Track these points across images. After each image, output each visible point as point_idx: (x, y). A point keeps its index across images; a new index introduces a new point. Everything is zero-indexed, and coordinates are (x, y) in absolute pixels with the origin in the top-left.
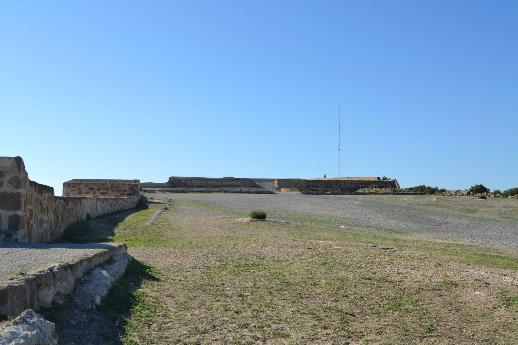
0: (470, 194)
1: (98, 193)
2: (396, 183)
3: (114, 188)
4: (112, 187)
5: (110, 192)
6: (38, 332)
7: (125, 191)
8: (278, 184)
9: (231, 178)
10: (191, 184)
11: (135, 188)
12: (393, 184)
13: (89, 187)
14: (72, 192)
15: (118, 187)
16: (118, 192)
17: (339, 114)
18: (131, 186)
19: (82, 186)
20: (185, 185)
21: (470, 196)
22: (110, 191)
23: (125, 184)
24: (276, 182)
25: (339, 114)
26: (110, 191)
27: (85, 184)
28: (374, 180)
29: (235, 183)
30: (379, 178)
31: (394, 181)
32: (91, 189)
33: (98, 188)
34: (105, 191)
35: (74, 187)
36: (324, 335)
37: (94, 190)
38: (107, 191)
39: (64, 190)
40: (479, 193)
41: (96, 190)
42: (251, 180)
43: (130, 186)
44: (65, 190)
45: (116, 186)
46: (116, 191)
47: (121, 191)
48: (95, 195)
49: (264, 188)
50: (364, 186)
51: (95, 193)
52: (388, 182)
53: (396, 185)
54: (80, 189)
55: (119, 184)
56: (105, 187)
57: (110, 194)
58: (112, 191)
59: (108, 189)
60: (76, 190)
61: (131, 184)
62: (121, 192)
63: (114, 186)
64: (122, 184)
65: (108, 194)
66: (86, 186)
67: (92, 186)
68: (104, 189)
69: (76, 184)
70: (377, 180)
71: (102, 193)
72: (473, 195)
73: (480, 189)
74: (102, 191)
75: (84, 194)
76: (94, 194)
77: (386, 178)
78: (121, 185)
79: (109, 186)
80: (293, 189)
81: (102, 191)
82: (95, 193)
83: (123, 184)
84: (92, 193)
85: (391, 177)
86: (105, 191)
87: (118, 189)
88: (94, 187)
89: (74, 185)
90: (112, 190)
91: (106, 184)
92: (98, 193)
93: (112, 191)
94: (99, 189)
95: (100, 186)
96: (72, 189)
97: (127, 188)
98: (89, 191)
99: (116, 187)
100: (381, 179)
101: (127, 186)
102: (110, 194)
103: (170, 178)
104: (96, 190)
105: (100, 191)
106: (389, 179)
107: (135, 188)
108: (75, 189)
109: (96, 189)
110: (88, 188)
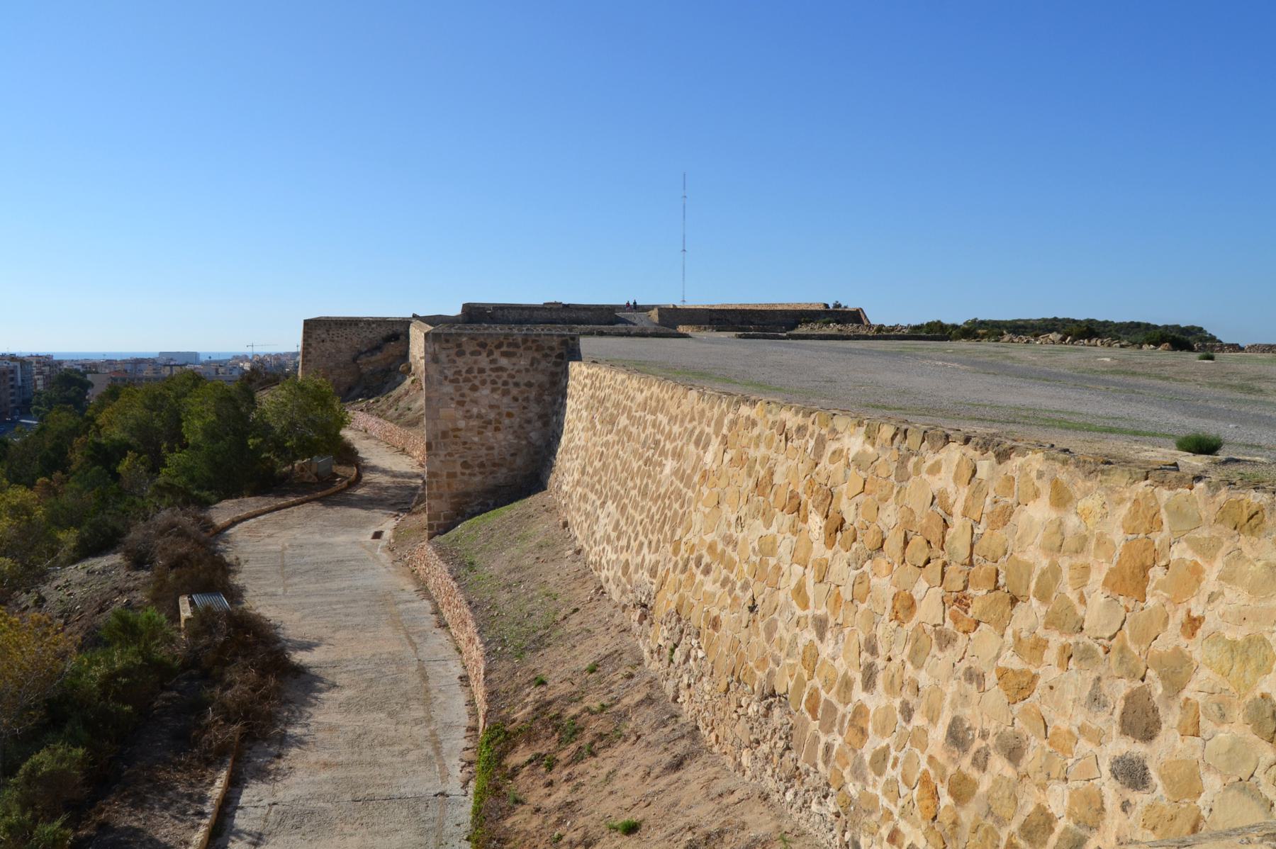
0: (1067, 341)
1: (496, 354)
2: (861, 314)
3: (529, 344)
4: (525, 341)
5: (521, 351)
6: (96, 693)
7: (552, 348)
8: (660, 316)
9: (555, 304)
10: (503, 316)
11: (571, 342)
12: (856, 316)
13: (479, 341)
14: (444, 352)
15: (538, 341)
16: (537, 350)
17: (684, 189)
18: (564, 338)
19: (464, 339)
20: (492, 318)
21: (1066, 344)
22: (522, 348)
23: (552, 335)
24: (654, 314)
25: (684, 189)
26: (522, 348)
27: (469, 334)
28: (818, 308)
29: (583, 315)
30: (827, 306)
31: (858, 310)
32: (483, 345)
33: (496, 343)
34: (511, 349)
35: (447, 341)
36: (653, 594)
37: (488, 348)
38: (515, 350)
39: (428, 349)
40: (1084, 339)
41: (493, 348)
42: (611, 309)
43: (560, 339)
44: (430, 347)
45: (534, 338)
46: (534, 348)
47: (543, 349)
48: (491, 358)
49: (634, 324)
50: (807, 319)
51: (490, 353)
52: (843, 311)
53: (863, 318)
54: (459, 345)
55: (540, 335)
56: (511, 341)
57: (521, 355)
58: (525, 349)
59: (517, 346)
60: (452, 348)
61: (564, 335)
62: (544, 352)
63: (530, 339)
64: (545, 335)
65: (518, 355)
66: (472, 339)
67: (485, 339)
68: (509, 345)
69: (451, 334)
70: (822, 308)
71: (505, 354)
72: (1072, 344)
73: (1085, 332)
74: (504, 349)
75: (469, 356)
76: (488, 356)
77: (840, 306)
78: (543, 337)
79: (520, 339)
80: (703, 326)
81: (504, 349)
82: (490, 353)
83: (547, 335)
84: (485, 354)
85: (851, 304)
86: (511, 349)
87: (538, 346)
88: (489, 341)
89: (448, 338)
90: (524, 346)
91: (512, 335)
92: (496, 354)
93: (525, 349)
94: (499, 346)
95: (502, 339)
96: (445, 345)
97: (554, 344)
98: (478, 348)
99: (534, 341)
100: (831, 306)
101: (555, 338)
102: (521, 355)
103: (464, 305)
104: (493, 348)
105: (502, 350)
106: (846, 307)
107: (571, 342)
108: (449, 345)
109: (493, 345)
110: (475, 342)
